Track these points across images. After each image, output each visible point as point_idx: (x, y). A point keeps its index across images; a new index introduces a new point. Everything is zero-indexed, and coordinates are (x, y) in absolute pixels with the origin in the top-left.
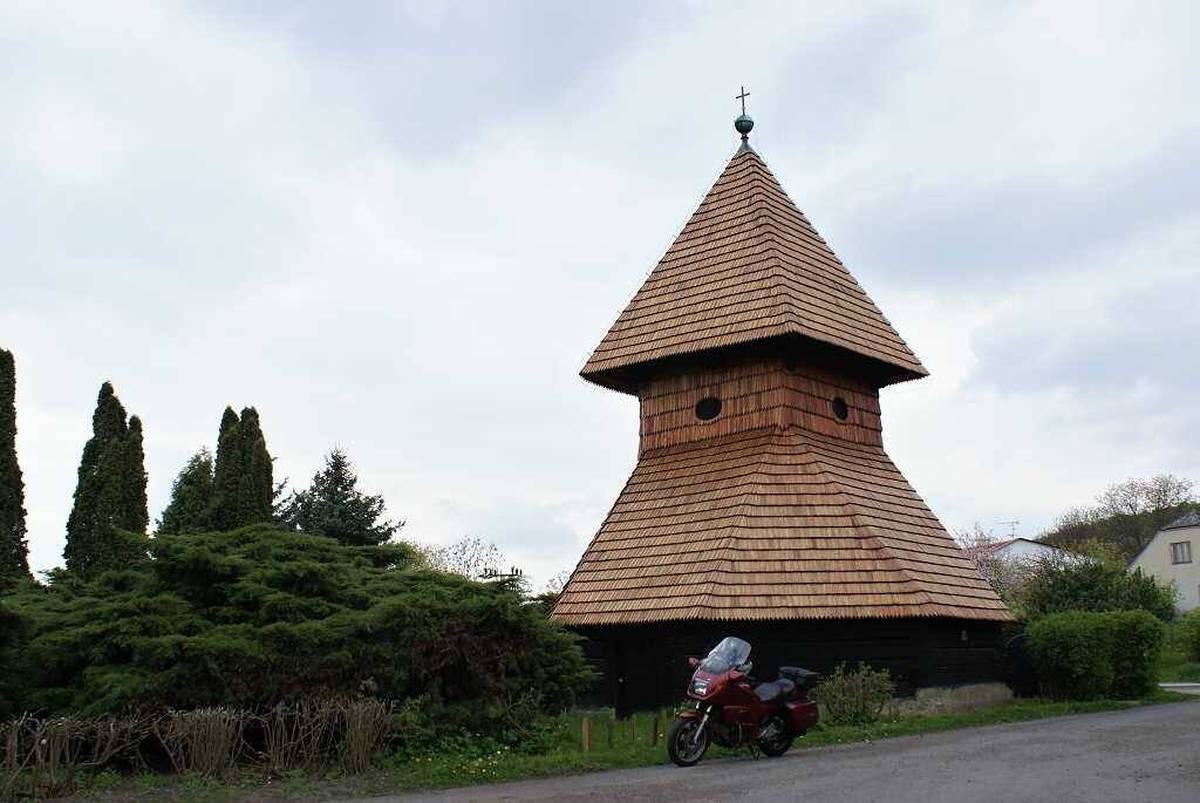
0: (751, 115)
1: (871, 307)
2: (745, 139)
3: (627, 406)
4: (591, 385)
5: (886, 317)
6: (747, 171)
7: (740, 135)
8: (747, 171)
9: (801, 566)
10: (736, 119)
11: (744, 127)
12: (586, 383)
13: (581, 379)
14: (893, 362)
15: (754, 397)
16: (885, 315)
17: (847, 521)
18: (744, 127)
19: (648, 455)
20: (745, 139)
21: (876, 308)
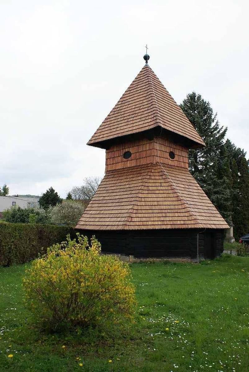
0: (149, 54)
1: (170, 96)
2: (147, 62)
3: (102, 153)
4: (92, 147)
5: (167, 90)
6: (146, 71)
7: (145, 61)
8: (146, 71)
9: (162, 188)
10: (144, 55)
11: (146, 58)
12: (90, 146)
13: (88, 146)
14: (167, 129)
15: (112, 159)
16: (160, 79)
17: (170, 188)
18: (146, 58)
19: (107, 172)
20: (147, 62)
21: (174, 101)
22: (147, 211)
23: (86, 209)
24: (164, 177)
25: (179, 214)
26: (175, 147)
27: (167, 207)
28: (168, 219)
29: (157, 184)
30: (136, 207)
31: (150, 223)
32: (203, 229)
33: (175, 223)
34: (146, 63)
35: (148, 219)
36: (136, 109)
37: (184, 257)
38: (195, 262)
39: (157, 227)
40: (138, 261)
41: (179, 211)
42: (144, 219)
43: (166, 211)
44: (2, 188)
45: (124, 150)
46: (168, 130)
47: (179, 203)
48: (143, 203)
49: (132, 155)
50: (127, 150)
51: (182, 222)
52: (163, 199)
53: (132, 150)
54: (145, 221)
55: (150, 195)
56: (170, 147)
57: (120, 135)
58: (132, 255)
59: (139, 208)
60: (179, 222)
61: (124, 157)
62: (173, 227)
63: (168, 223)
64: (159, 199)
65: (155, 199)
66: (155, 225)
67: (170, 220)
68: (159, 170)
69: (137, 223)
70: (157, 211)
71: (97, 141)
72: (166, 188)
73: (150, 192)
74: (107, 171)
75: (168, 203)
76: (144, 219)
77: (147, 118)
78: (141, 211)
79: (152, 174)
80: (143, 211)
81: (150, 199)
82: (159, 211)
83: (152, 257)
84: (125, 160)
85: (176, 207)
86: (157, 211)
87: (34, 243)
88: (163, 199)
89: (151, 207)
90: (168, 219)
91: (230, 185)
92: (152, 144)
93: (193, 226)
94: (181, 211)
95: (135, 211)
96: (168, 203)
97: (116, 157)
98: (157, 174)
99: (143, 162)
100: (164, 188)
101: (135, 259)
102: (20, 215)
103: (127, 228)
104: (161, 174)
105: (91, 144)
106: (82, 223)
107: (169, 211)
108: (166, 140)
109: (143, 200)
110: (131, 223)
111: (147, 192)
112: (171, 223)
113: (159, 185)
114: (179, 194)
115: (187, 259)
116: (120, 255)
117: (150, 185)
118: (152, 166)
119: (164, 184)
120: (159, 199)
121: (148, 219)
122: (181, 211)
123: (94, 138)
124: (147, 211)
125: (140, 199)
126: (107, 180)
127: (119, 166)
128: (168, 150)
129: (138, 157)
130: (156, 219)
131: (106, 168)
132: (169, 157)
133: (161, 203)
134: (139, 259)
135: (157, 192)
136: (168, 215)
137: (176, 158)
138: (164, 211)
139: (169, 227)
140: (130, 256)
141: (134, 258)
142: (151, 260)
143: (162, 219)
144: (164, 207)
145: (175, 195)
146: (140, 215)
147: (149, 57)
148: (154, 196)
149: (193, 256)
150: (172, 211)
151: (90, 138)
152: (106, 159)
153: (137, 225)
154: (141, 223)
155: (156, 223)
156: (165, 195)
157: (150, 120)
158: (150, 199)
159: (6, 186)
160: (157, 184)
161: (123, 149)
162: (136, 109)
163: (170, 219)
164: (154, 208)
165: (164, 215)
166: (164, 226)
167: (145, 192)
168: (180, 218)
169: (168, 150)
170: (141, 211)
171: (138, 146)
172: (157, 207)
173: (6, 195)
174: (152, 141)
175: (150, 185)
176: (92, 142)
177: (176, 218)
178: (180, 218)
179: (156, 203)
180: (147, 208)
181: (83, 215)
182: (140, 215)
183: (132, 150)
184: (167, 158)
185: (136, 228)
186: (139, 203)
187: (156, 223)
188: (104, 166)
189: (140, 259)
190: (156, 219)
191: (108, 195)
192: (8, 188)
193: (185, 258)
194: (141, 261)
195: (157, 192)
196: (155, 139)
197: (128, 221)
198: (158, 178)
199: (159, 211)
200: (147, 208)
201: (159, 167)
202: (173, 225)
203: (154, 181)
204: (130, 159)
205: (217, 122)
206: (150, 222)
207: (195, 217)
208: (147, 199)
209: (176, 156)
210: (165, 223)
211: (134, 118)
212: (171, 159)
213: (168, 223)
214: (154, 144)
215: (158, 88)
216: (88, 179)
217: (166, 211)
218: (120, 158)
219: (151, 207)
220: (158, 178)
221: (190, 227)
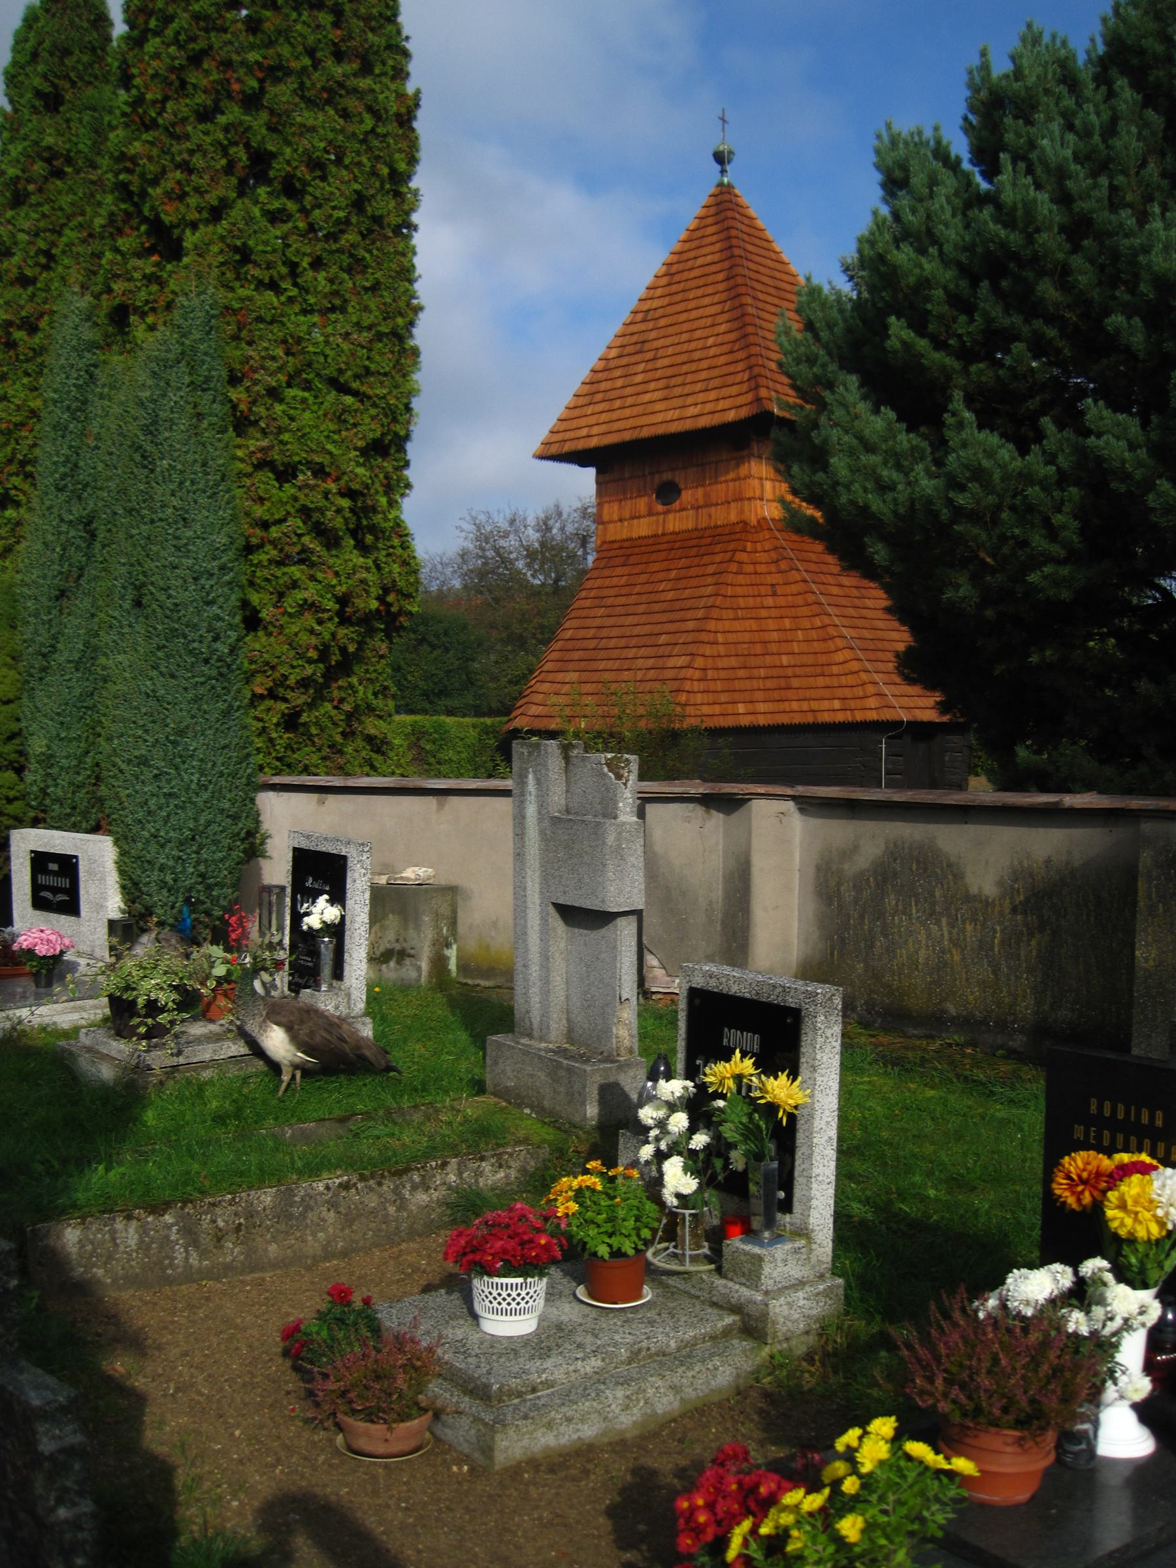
2: (723, 172)
6: (724, 208)
8: (724, 208)
11: (720, 158)
20: (723, 172)
23: (545, 668)
24: (783, 565)
36: (693, 345)
45: (657, 477)
50: (667, 476)
71: (568, 447)
74: (604, 542)
77: (730, 380)
84: (660, 508)
87: (364, 754)
106: (534, 710)
107: (798, 671)
123: (559, 437)
126: (607, 572)
127: (643, 528)
129: (701, 502)
151: (542, 434)
157: (734, 390)
161: (652, 474)
162: (693, 345)
175: (739, 591)
176: (554, 449)
191: (611, 621)
204: (677, 505)
211: (689, 378)
215: (762, 269)
216: (482, 518)
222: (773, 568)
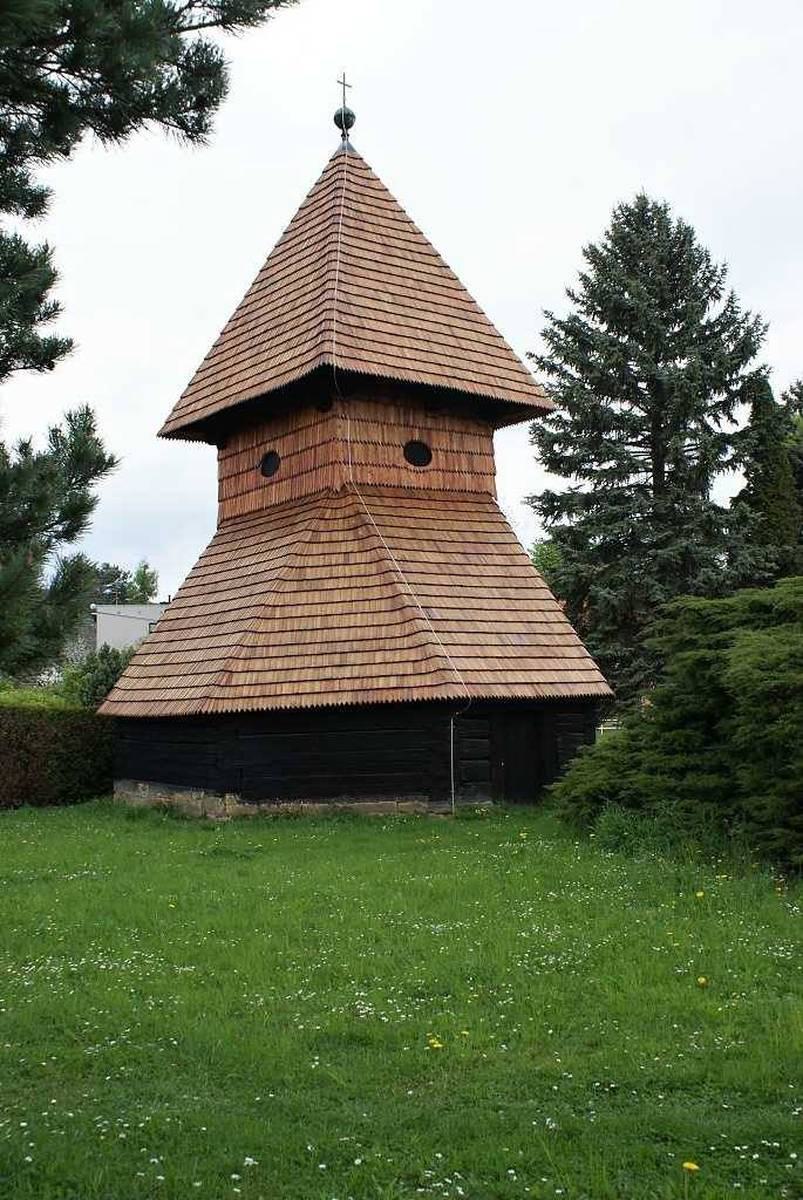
3: (204, 457)
9: (347, 571)
11: (344, 120)
17: (373, 569)
18: (344, 120)
22: (283, 651)
25: (389, 656)
26: (429, 424)
27: (352, 634)
28: (347, 672)
29: (334, 559)
30: (249, 640)
31: (286, 689)
32: (460, 702)
33: (367, 684)
34: (343, 140)
35: (282, 676)
37: (404, 798)
38: (442, 810)
39: (307, 702)
40: (253, 813)
41: (389, 644)
42: (269, 677)
43: (346, 647)
44: (134, 576)
45: (262, 447)
46: (250, 400)
47: (397, 616)
48: (277, 625)
49: (282, 465)
50: (269, 447)
51: (393, 682)
52: (346, 608)
53: (280, 448)
54: (271, 683)
55: (303, 598)
56: (406, 425)
57: (231, 402)
58: (234, 791)
59: (262, 640)
60: (382, 683)
61: (264, 474)
62: (361, 698)
63: (347, 685)
64: (329, 609)
65: (318, 610)
66: (302, 694)
67: (356, 674)
68: (348, 511)
69: (245, 691)
70: (317, 649)
72: (362, 569)
73: (305, 586)
75: (358, 620)
76: (269, 677)
78: (263, 652)
79: (322, 525)
80: (273, 652)
81: (299, 611)
82: (325, 648)
83: (289, 798)
84: (264, 480)
85: (383, 632)
86: (317, 649)
88: (346, 608)
89: (297, 637)
90: (347, 672)
91: (788, 529)
92: (330, 421)
93: (427, 694)
94: (398, 643)
95: (244, 653)
96: (358, 620)
97: (243, 472)
98: (340, 524)
99: (309, 484)
100: (354, 570)
101: (241, 806)
102: (105, 671)
103: (209, 707)
104: (353, 522)
105: (159, 435)
107: (356, 646)
108: (386, 405)
109: (278, 613)
110: (228, 692)
111: (294, 586)
112: (357, 684)
113: (341, 561)
114: (401, 588)
115: (416, 802)
116: (203, 793)
117: (310, 561)
118: (328, 498)
119: (359, 558)
120: (329, 609)
121: (282, 676)
122: (398, 643)
124: (283, 651)
125: (269, 612)
127: (252, 502)
128: (399, 437)
130: (310, 674)
131: (222, 510)
132: (403, 462)
133: (334, 622)
134: (256, 806)
135: (330, 584)
136: (352, 658)
137: (439, 459)
138: (339, 647)
139: (346, 699)
140: (227, 797)
141: (239, 803)
142: (291, 806)
143: (328, 673)
144: (344, 634)
145: (388, 592)
146: (258, 665)
147: (353, 116)
148: (317, 597)
149: (436, 791)
150: (368, 645)
152: (220, 481)
153: (245, 698)
154: (258, 691)
155: (307, 687)
156: (354, 594)
158: (299, 611)
159: (146, 567)
160: (334, 559)
163: (356, 671)
164: (308, 637)
165: (337, 659)
166: (331, 696)
167: (288, 587)
168: (388, 669)
169: (399, 437)
170: (263, 652)
171: (294, 432)
172: (319, 636)
173: (151, 600)
174: (329, 414)
176: (170, 427)
177: (375, 670)
178: (388, 669)
179: (318, 623)
180: (287, 638)
181: (129, 671)
182: (258, 665)
183: (280, 448)
184: (394, 466)
185: (241, 706)
186: (263, 626)
187: (307, 687)
188: (215, 505)
189: (258, 804)
190: (310, 674)
192: (153, 574)
193: (407, 800)
194: (263, 813)
195: (330, 584)
196: (337, 405)
197: (219, 685)
198: (340, 536)
199: (325, 648)
200: (287, 638)
201: (350, 500)
202: (360, 694)
203: (327, 548)
204: (276, 476)
205: (731, 300)
206: (288, 685)
207: (441, 663)
208: (288, 611)
209: (437, 458)
210: (336, 686)
212: (412, 467)
213: (347, 685)
214: (334, 423)
217: (346, 647)
218: (252, 474)
219: (297, 637)
220: (340, 536)
221: (416, 695)
222: (350, 535)
